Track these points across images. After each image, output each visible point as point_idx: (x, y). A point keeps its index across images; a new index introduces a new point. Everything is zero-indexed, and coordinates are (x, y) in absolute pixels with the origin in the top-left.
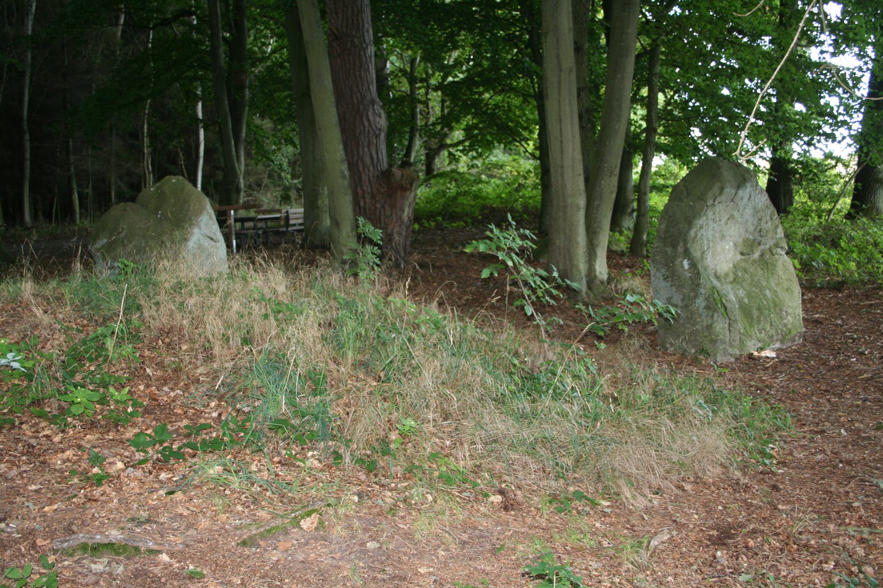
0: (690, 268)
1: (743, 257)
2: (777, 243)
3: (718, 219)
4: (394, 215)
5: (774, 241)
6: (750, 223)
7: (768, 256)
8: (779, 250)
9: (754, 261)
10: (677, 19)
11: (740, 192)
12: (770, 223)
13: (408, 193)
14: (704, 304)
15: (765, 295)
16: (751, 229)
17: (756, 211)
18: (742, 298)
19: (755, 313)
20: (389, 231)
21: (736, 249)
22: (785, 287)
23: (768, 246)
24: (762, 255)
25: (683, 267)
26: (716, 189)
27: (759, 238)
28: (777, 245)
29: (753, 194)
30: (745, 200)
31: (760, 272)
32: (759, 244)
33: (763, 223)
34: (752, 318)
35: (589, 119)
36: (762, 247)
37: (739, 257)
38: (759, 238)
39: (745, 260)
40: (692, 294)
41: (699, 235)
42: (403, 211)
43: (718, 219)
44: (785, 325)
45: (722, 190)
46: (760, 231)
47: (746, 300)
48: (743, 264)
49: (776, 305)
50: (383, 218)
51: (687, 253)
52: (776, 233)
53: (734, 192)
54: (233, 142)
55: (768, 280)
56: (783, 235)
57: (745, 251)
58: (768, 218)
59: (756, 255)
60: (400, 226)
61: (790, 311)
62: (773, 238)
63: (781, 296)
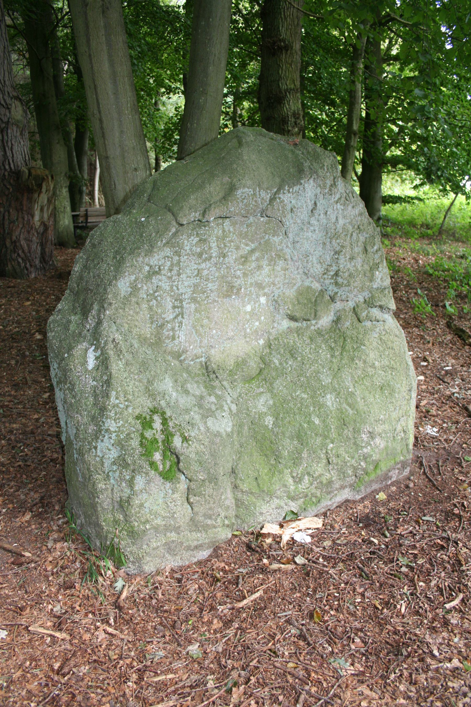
0: (97, 368)
1: (294, 325)
2: (372, 297)
3: (214, 252)
4: (20, 219)
5: (366, 294)
6: (314, 259)
7: (348, 324)
8: (375, 312)
9: (319, 333)
10: (453, 60)
11: (287, 198)
12: (359, 261)
13: (36, 195)
14: (114, 454)
15: (321, 406)
16: (318, 269)
17: (331, 235)
18: (261, 415)
19: (287, 446)
20: (14, 238)
21: (277, 309)
22: (378, 382)
23: (351, 304)
24: (337, 321)
25: (85, 362)
26: (215, 189)
27: (332, 289)
28: (370, 303)
29: (321, 203)
30: (304, 214)
31: (325, 354)
32: (332, 299)
33: (343, 261)
34: (278, 458)
35: (295, 123)
36: (338, 305)
37: (286, 324)
38: (332, 289)
39: (298, 331)
40: (91, 428)
41: (145, 289)
42: (33, 216)
43: (214, 252)
44: (365, 458)
45: (231, 190)
46: (337, 274)
47: (269, 421)
48: (292, 339)
49: (343, 423)
50: (7, 223)
51: (96, 337)
52: (371, 280)
53: (267, 196)
54: (75, 154)
55: (336, 373)
56: (388, 282)
57: (298, 315)
58: (358, 249)
59: (325, 321)
60: (29, 232)
61: (379, 429)
62: (362, 289)
63: (361, 404)
